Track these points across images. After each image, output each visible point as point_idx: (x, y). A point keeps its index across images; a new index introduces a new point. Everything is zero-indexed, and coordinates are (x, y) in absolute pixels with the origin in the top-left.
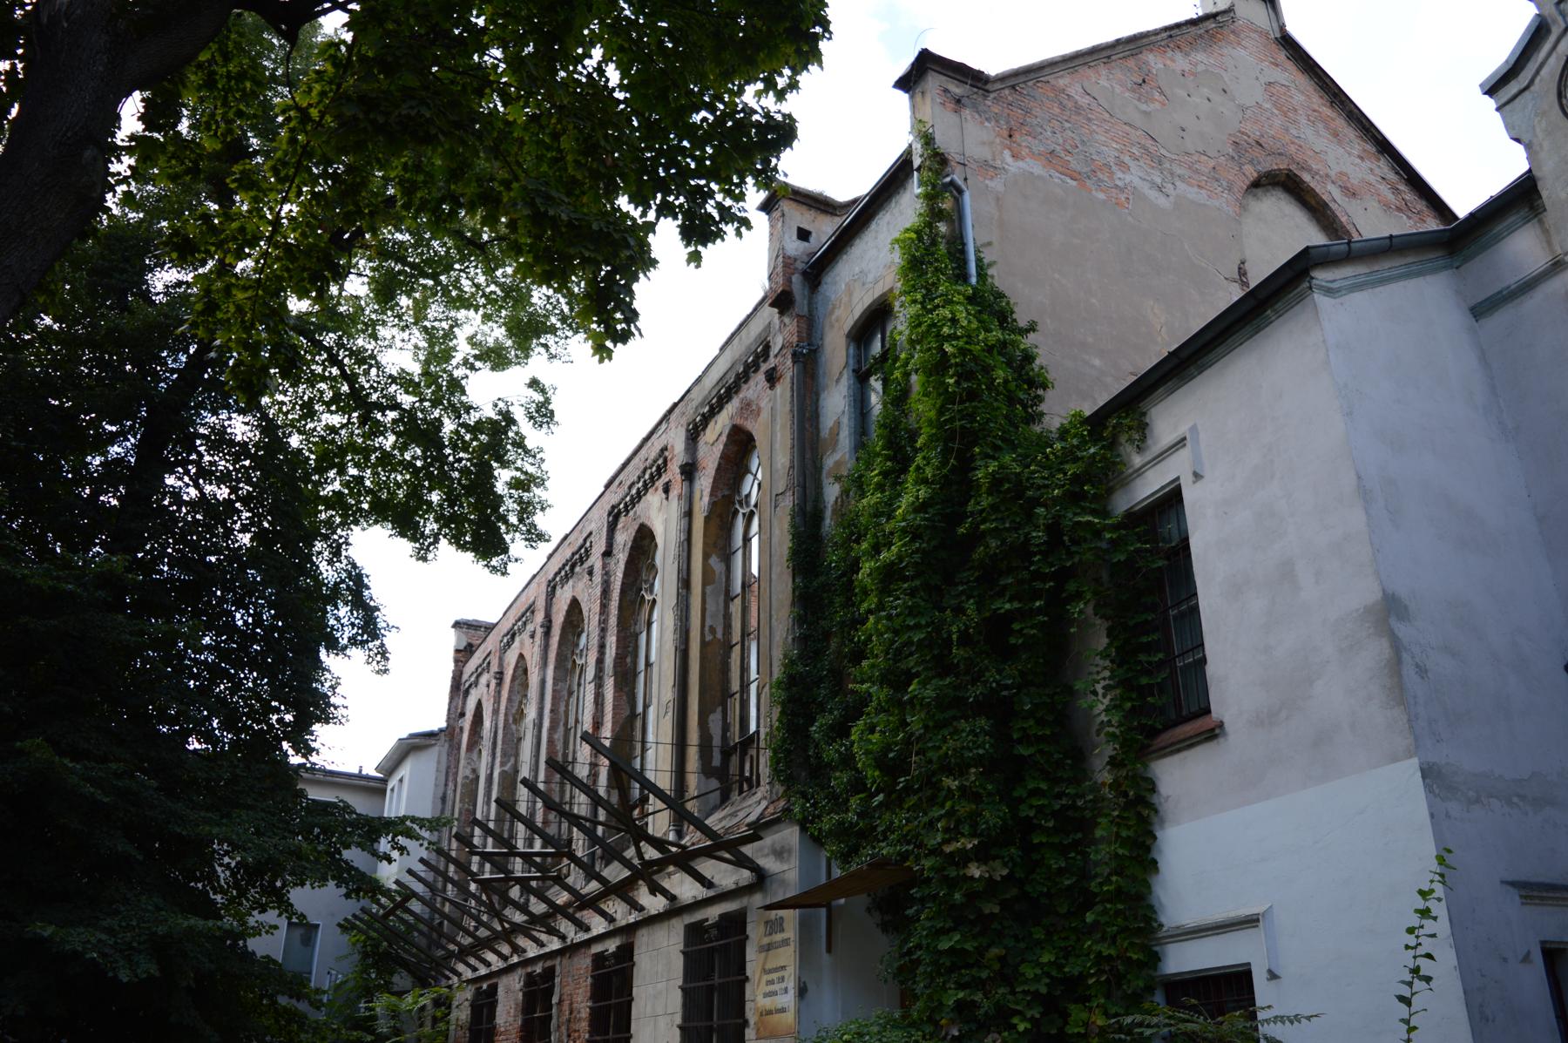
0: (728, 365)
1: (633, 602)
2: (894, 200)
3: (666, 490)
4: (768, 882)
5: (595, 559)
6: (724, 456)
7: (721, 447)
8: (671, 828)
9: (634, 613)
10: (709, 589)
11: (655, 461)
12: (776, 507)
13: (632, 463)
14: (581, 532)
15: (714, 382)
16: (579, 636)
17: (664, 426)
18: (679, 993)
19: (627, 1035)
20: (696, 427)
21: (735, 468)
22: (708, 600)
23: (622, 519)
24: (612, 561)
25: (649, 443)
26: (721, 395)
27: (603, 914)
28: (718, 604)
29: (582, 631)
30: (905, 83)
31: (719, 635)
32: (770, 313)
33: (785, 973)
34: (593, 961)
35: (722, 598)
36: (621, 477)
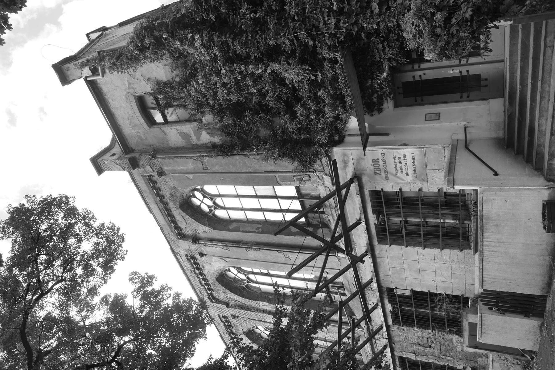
0: (156, 206)
1: (248, 292)
2: (105, 96)
3: (202, 255)
4: (358, 172)
6: (191, 216)
8: (336, 255)
10: (241, 229)
12: (208, 170)
13: (193, 282)
14: (219, 324)
15: (162, 217)
16: (262, 337)
19: (428, 294)
24: (232, 303)
29: (260, 334)
30: (100, 171)
31: (260, 226)
32: (135, 172)
33: (397, 156)
34: (396, 325)
36: (198, 291)
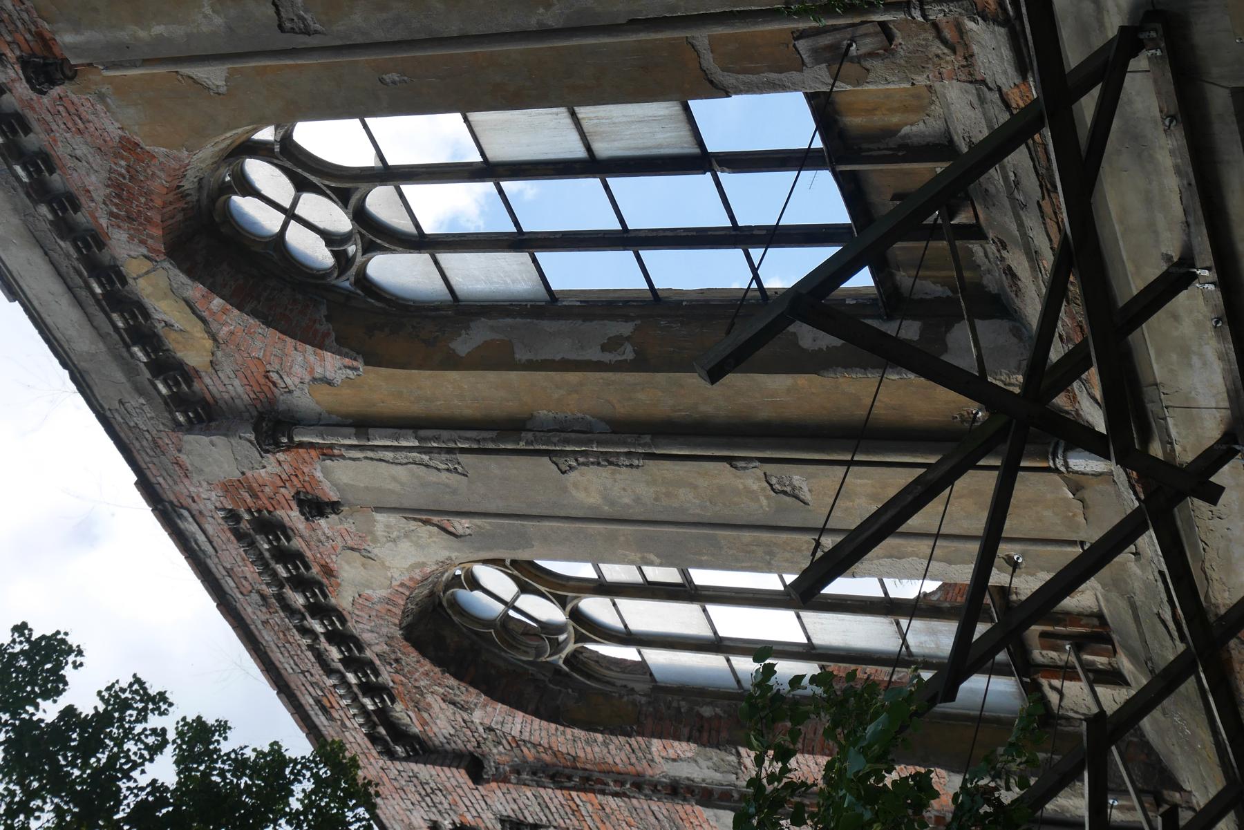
0: (37, 257)
3: (315, 507)
6: (239, 300)
8: (1059, 462)
10: (521, 355)
11: (260, 559)
12: (307, 32)
24: (497, 754)
31: (626, 329)
35: (547, 325)
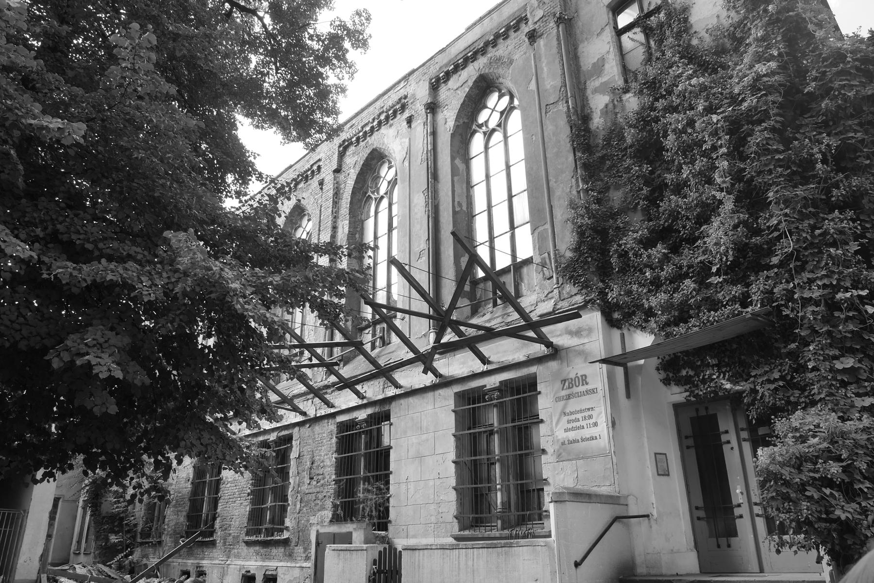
1: (360, 201)
3: (409, 121)
4: (563, 353)
5: (327, 174)
7: (467, 90)
8: (432, 330)
9: (360, 207)
10: (456, 179)
13: (366, 112)
14: (308, 161)
17: (402, 84)
18: (453, 439)
20: (438, 80)
21: (474, 106)
22: (456, 185)
23: (352, 149)
24: (341, 177)
25: (386, 97)
26: (468, 57)
27: (357, 393)
28: (462, 189)
31: (464, 208)
34: (337, 427)
35: (465, 185)
36: (353, 121)
